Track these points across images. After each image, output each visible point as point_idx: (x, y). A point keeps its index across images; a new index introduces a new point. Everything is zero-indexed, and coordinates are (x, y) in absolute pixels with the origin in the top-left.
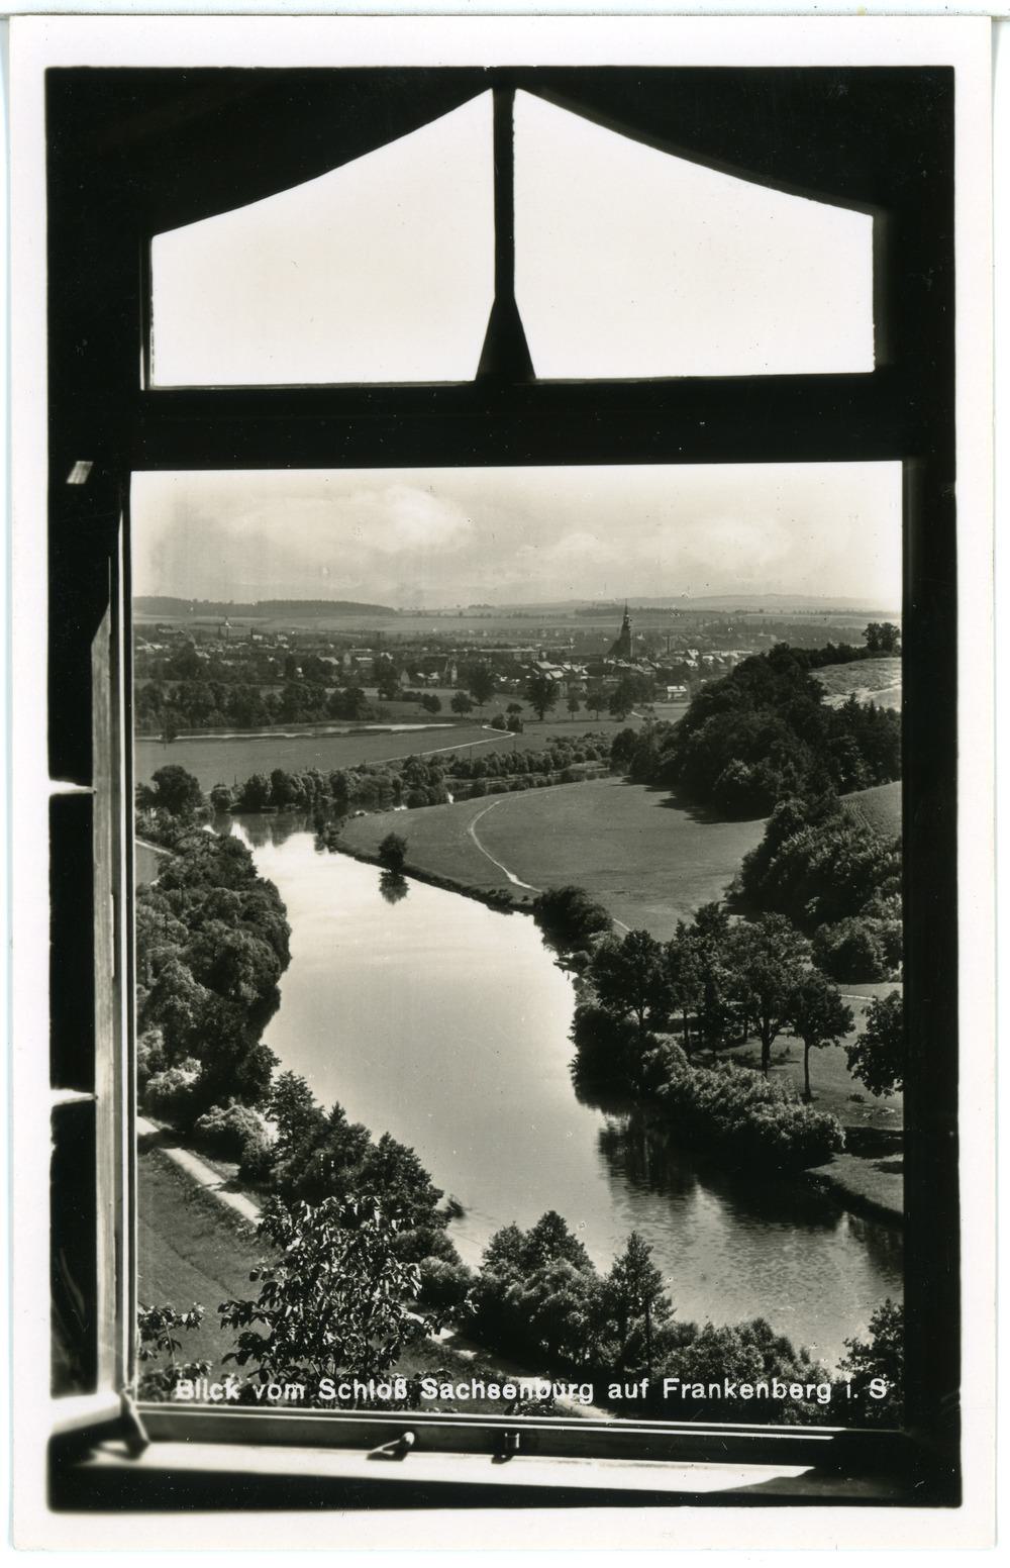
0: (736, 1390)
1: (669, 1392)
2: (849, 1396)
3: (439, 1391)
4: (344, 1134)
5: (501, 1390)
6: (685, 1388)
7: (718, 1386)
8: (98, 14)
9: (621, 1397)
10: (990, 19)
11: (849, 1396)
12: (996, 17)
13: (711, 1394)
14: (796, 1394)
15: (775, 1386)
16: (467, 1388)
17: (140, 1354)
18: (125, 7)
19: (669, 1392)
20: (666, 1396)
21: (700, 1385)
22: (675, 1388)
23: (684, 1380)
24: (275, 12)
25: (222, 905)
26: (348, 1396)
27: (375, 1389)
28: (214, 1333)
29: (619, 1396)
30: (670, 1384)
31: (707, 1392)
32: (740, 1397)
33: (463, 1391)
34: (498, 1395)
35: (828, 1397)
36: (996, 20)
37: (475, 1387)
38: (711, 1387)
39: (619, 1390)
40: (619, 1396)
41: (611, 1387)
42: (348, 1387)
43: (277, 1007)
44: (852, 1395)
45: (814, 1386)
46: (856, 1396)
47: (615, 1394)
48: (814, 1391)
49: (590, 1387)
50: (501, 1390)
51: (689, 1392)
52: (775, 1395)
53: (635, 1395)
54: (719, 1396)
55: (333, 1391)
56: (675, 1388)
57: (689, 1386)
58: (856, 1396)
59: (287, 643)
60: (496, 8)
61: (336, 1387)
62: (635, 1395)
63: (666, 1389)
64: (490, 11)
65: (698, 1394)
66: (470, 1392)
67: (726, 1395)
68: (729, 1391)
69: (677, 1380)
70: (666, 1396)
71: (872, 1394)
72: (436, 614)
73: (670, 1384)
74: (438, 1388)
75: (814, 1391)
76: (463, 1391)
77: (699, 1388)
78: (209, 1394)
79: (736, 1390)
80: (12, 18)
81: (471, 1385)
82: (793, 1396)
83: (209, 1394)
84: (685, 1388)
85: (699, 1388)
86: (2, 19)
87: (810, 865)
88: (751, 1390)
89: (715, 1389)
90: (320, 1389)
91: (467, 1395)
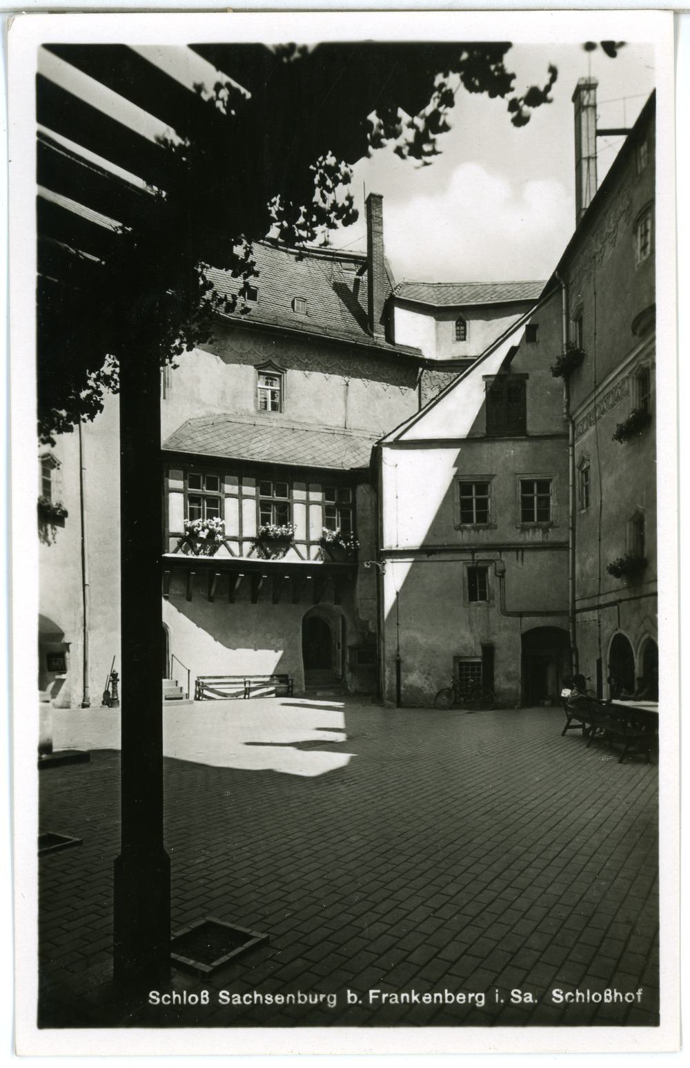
1: (373, 999)
3: (231, 999)
6: (384, 996)
7: (407, 995)
8: (577, 10)
10: (672, 12)
13: (615, 999)
14: (461, 1000)
19: (373, 999)
20: (371, 1001)
21: (528, 994)
22: (377, 997)
23: (383, 991)
24: (513, 7)
26: (169, 1002)
27: (591, 995)
29: (239, 1002)
30: (374, 994)
31: (399, 1000)
32: (243, 1004)
35: (483, 1002)
38: (436, 995)
41: (426, 994)
44: (499, 1000)
45: (473, 995)
46: (360, 1002)
47: (394, 1000)
48: (473, 998)
49: (335, 996)
50: (274, 998)
51: (387, 999)
52: (447, 1001)
53: (436, 995)
54: (180, 1002)
55: (158, 1000)
56: (377, 997)
58: (502, 1001)
61: (160, 997)
63: (371, 997)
64: (539, 8)
65: (236, 1001)
67: (413, 1001)
69: (378, 991)
70: (371, 1001)
74: (230, 996)
76: (597, 997)
77: (428, 996)
78: (591, 998)
81: (172, 995)
85: (528, 996)
86: (1, 12)
88: (458, 998)
89: (405, 998)
91: (169, 1002)
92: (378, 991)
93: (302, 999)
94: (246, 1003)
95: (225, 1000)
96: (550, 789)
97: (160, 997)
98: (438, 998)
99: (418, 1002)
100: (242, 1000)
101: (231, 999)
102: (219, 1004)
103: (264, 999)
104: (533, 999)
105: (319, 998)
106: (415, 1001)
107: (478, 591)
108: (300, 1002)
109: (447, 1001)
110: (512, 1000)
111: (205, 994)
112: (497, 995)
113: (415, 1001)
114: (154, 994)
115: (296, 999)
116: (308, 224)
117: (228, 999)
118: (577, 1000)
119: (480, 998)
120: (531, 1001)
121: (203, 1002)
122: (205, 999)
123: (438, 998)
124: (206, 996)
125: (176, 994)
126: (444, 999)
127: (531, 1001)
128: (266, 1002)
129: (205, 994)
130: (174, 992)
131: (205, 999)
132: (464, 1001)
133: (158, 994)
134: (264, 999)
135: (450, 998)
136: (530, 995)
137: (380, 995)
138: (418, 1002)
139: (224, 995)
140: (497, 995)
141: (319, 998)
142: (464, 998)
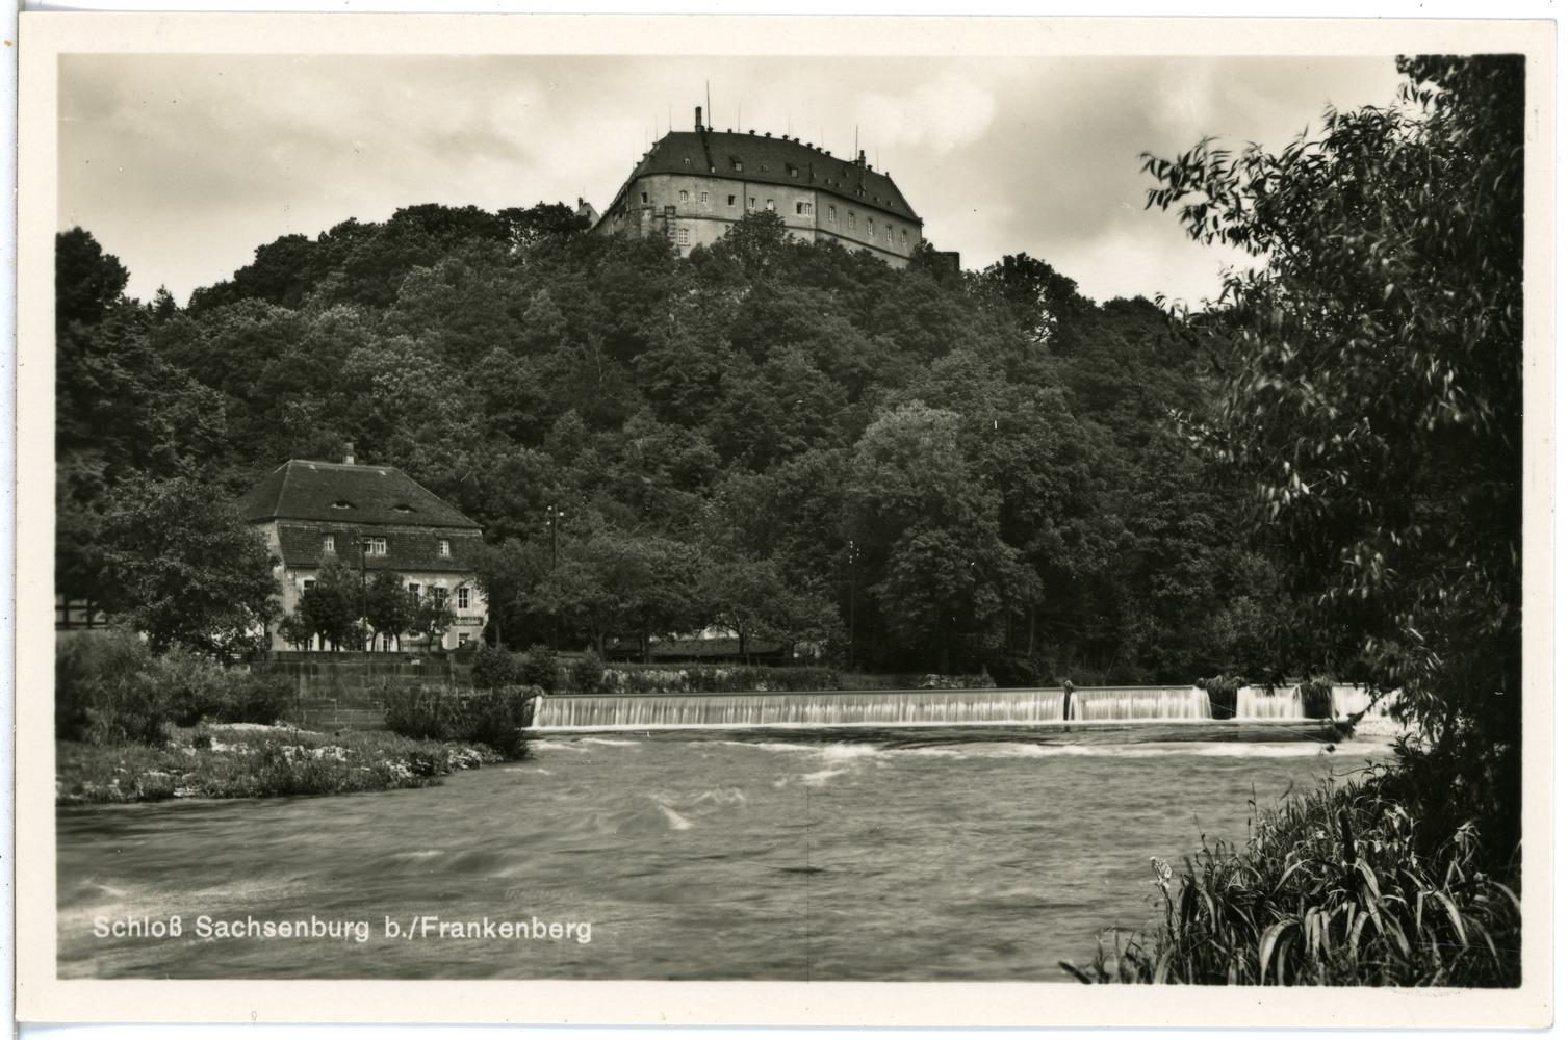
7: (305, 924)
12: (19, 5)
14: (556, 933)
15: (535, 926)
16: (243, 926)
18: (6, 921)
26: (242, 934)
32: (232, 937)
33: (238, 929)
35: (588, 935)
36: (23, 7)
37: (250, 926)
38: (298, 924)
43: (472, 208)
52: (535, 935)
53: (298, 924)
57: (447, 925)
60: (7, 932)
65: (221, 932)
66: (246, 929)
67: (485, 935)
68: (488, 930)
69: (435, 919)
71: (198, 931)
72: (61, 613)
73: (429, 923)
77: (221, 926)
78: (150, 930)
80: (19, 1018)
81: (246, 922)
82: (552, 935)
83: (150, 930)
85: (221, 926)
91: (242, 934)
92: (435, 919)
93: (319, 928)
100: (230, 929)
103: (262, 930)
105: (343, 933)
106: (489, 935)
108: (314, 933)
109: (535, 935)
114: (204, 921)
118: (130, 934)
119: (584, 930)
121: (172, 933)
122: (175, 928)
123: (474, 929)
124: (178, 925)
125: (318, 920)
126: (531, 932)
129: (175, 921)
130: (314, 918)
134: (262, 930)
135: (540, 931)
138: (494, 935)
141: (343, 933)
142: (561, 930)
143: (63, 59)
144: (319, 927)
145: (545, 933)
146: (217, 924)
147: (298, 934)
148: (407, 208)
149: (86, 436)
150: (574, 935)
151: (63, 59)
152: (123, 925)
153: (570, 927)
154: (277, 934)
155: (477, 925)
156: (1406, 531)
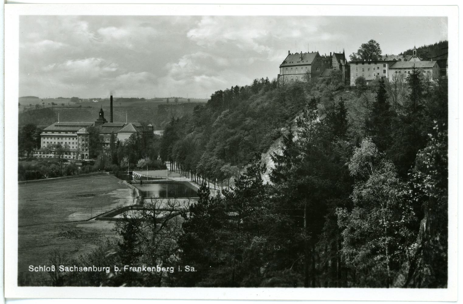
0: (146, 269)
2: (179, 271)
3: (65, 269)
4: (92, 240)
5: (83, 269)
6: (131, 268)
9: (69, 271)
11: (179, 271)
14: (149, 270)
15: (94, 268)
16: (73, 268)
17: (82, 228)
20: (125, 271)
25: (214, 182)
26: (38, 271)
27: (46, 268)
28: (375, 151)
29: (68, 270)
30: (126, 267)
34: (82, 270)
35: (173, 271)
36: (6, 2)
39: (68, 269)
40: (68, 270)
42: (38, 268)
45: (105, 268)
47: (192, 270)
48: (105, 269)
50: (83, 269)
52: (94, 270)
55: (33, 269)
58: (181, 271)
59: (333, 134)
61: (34, 268)
62: (101, 270)
66: (39, 269)
68: (144, 269)
69: (128, 266)
71: (60, 270)
73: (126, 267)
74: (64, 268)
75: (105, 269)
76: (48, 269)
79: (146, 269)
81: (39, 268)
84: (131, 268)
85: (192, 268)
87: (371, 163)
88: (84, 269)
90: (29, 269)
91: (38, 271)
92: (128, 266)
93: (95, 269)
94: (36, 271)
95: (188, 270)
96: (135, 183)
97: (34, 268)
98: (154, 269)
99: (146, 271)
101: (190, 269)
102: (29, 271)
103: (79, 269)
104: (195, 270)
105: (102, 269)
106: (144, 270)
107: (147, 181)
108: (94, 270)
109: (157, 271)
110: (186, 270)
111: (53, 267)
112: (179, 268)
113: (144, 270)
114: (31, 267)
115: (156, 269)
116: (382, 234)
117: (189, 269)
120: (194, 271)
121: (52, 270)
122: (53, 269)
123: (90, 269)
124: (54, 268)
125: (76, 267)
127: (194, 271)
128: (80, 270)
129: (53, 267)
130: (75, 266)
131: (53, 269)
132: (150, 271)
133: (33, 267)
134: (79, 269)
136: (194, 269)
137: (129, 268)
139: (62, 268)
140: (179, 268)
141: (102, 269)
143: (446, 19)
144: (95, 269)
145: (97, 270)
146: (65, 268)
147: (89, 271)
148: (210, 98)
149: (85, 133)
150: (105, 271)
151: (446, 19)
152: (73, 268)
153: (104, 268)
154: (83, 270)
155: (141, 268)
156: (355, 205)
